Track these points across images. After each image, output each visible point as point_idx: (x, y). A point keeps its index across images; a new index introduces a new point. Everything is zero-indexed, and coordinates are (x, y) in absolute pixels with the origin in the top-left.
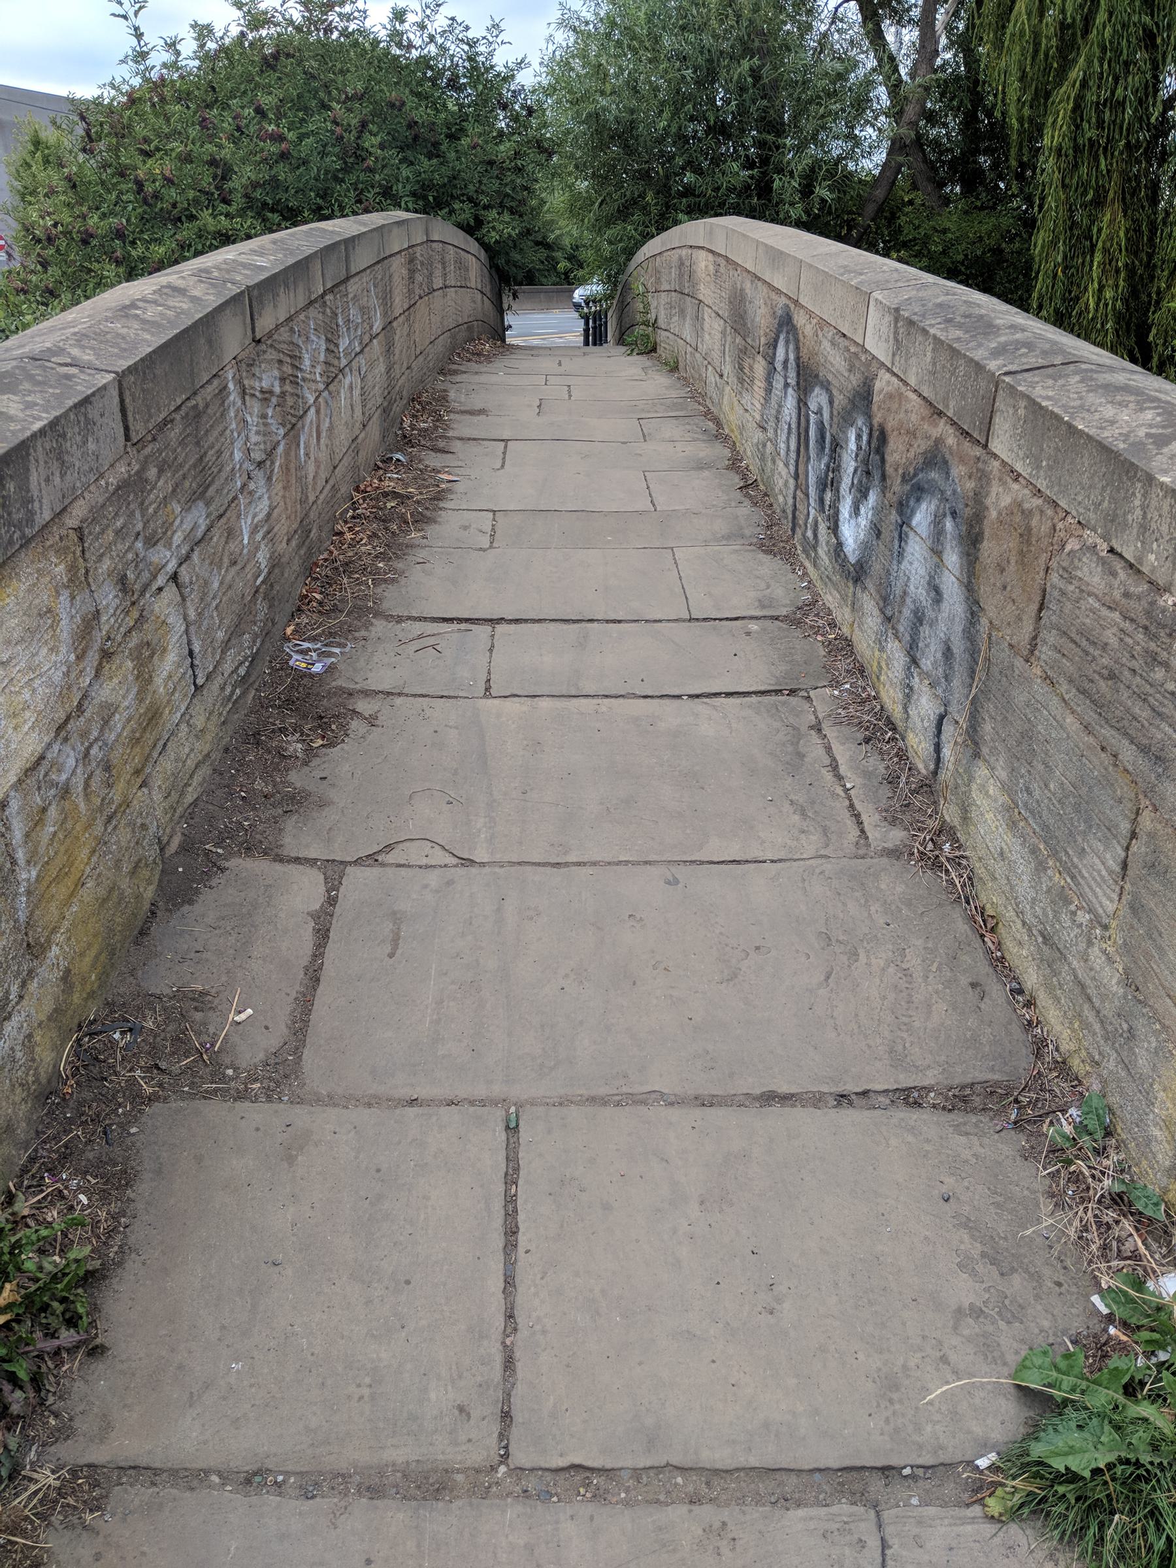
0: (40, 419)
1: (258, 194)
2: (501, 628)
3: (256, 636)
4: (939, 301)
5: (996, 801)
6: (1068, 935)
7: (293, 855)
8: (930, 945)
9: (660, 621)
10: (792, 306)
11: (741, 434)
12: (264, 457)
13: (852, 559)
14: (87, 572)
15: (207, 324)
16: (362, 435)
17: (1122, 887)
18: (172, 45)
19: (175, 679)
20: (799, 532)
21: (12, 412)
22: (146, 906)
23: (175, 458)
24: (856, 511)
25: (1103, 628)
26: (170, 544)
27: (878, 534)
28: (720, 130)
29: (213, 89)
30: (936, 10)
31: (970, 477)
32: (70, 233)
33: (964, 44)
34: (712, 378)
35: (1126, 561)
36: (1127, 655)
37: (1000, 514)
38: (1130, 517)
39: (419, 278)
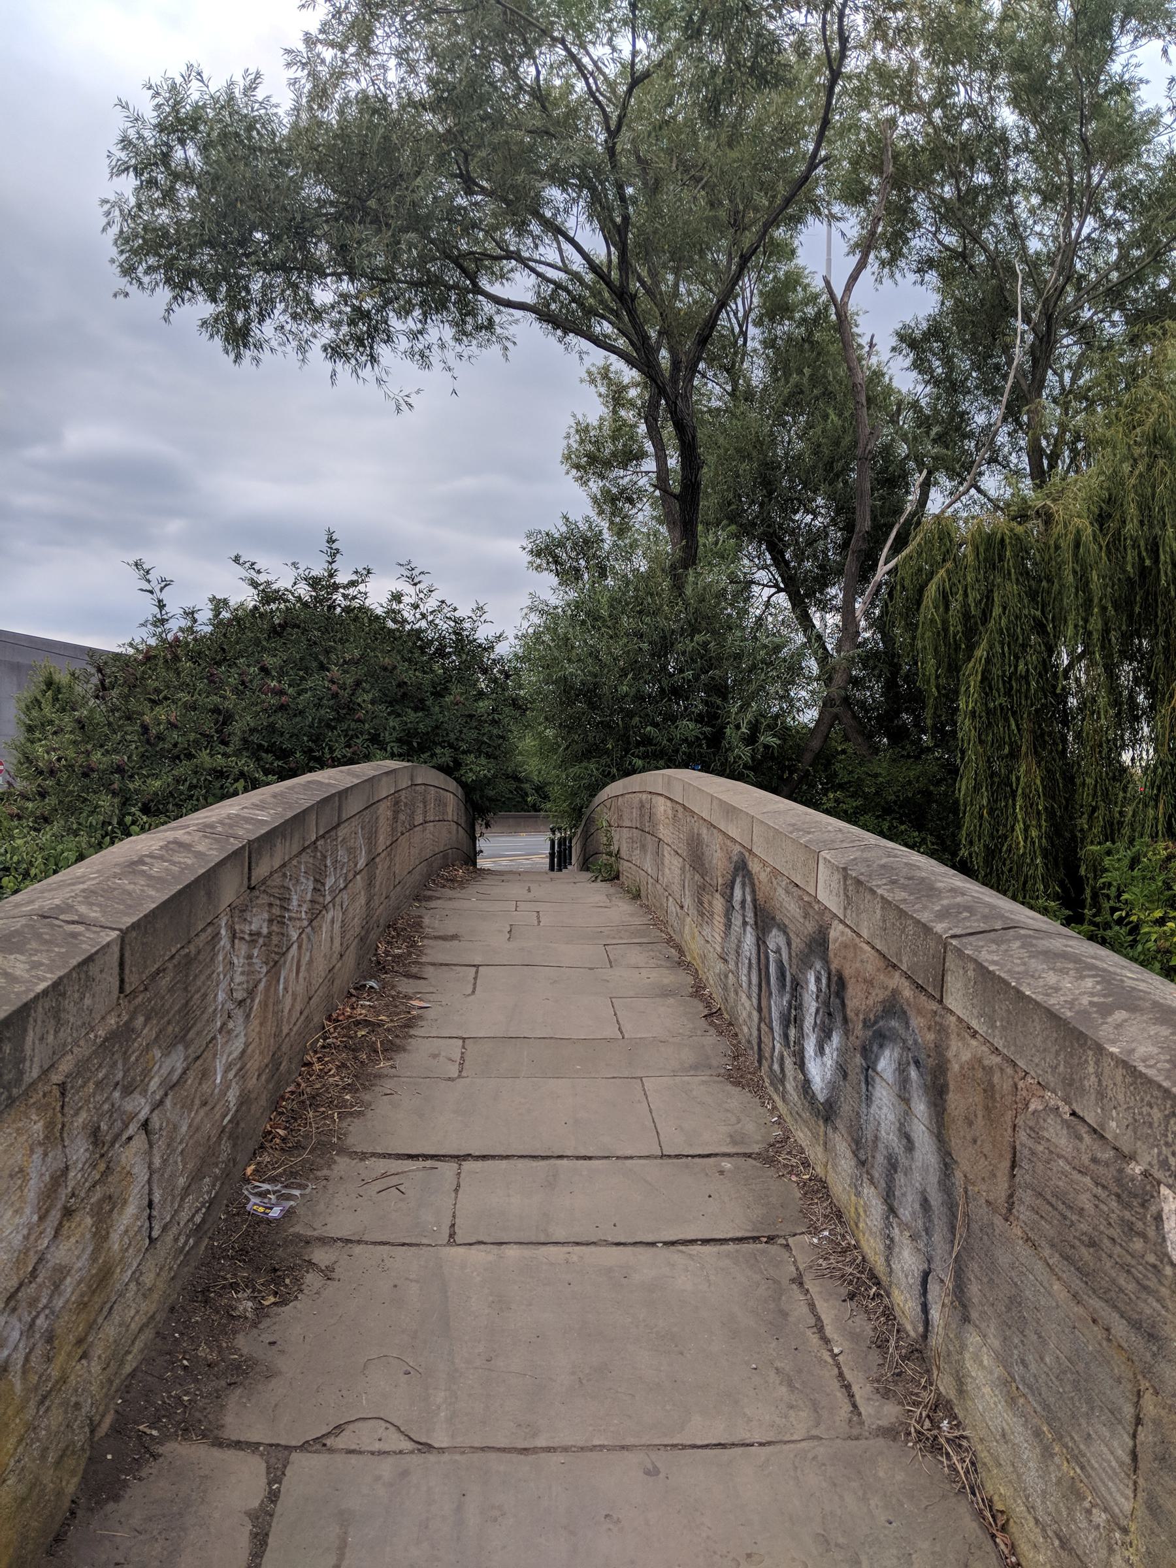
0: (44, 979)
1: (255, 738)
2: (468, 1165)
3: (216, 1178)
4: (883, 861)
6: (1086, 1540)
7: (234, 1438)
8: (938, 1549)
9: (631, 1158)
10: (747, 854)
11: (703, 962)
12: (245, 995)
13: (821, 1098)
14: (63, 1126)
15: (207, 882)
16: (339, 965)
17: (1135, 1483)
18: (190, 614)
19: (131, 1233)
20: (765, 1064)
21: (18, 973)
22: (67, 1504)
23: (163, 1005)
24: (821, 1051)
26: (146, 1091)
27: (845, 1076)
28: (677, 692)
29: (223, 650)
30: (855, 600)
31: (929, 1029)
32: (72, 766)
33: (881, 625)
34: (673, 908)
35: (1089, 1126)
36: (1105, 1223)
37: (962, 1067)
38: (1086, 1082)
39: (402, 817)
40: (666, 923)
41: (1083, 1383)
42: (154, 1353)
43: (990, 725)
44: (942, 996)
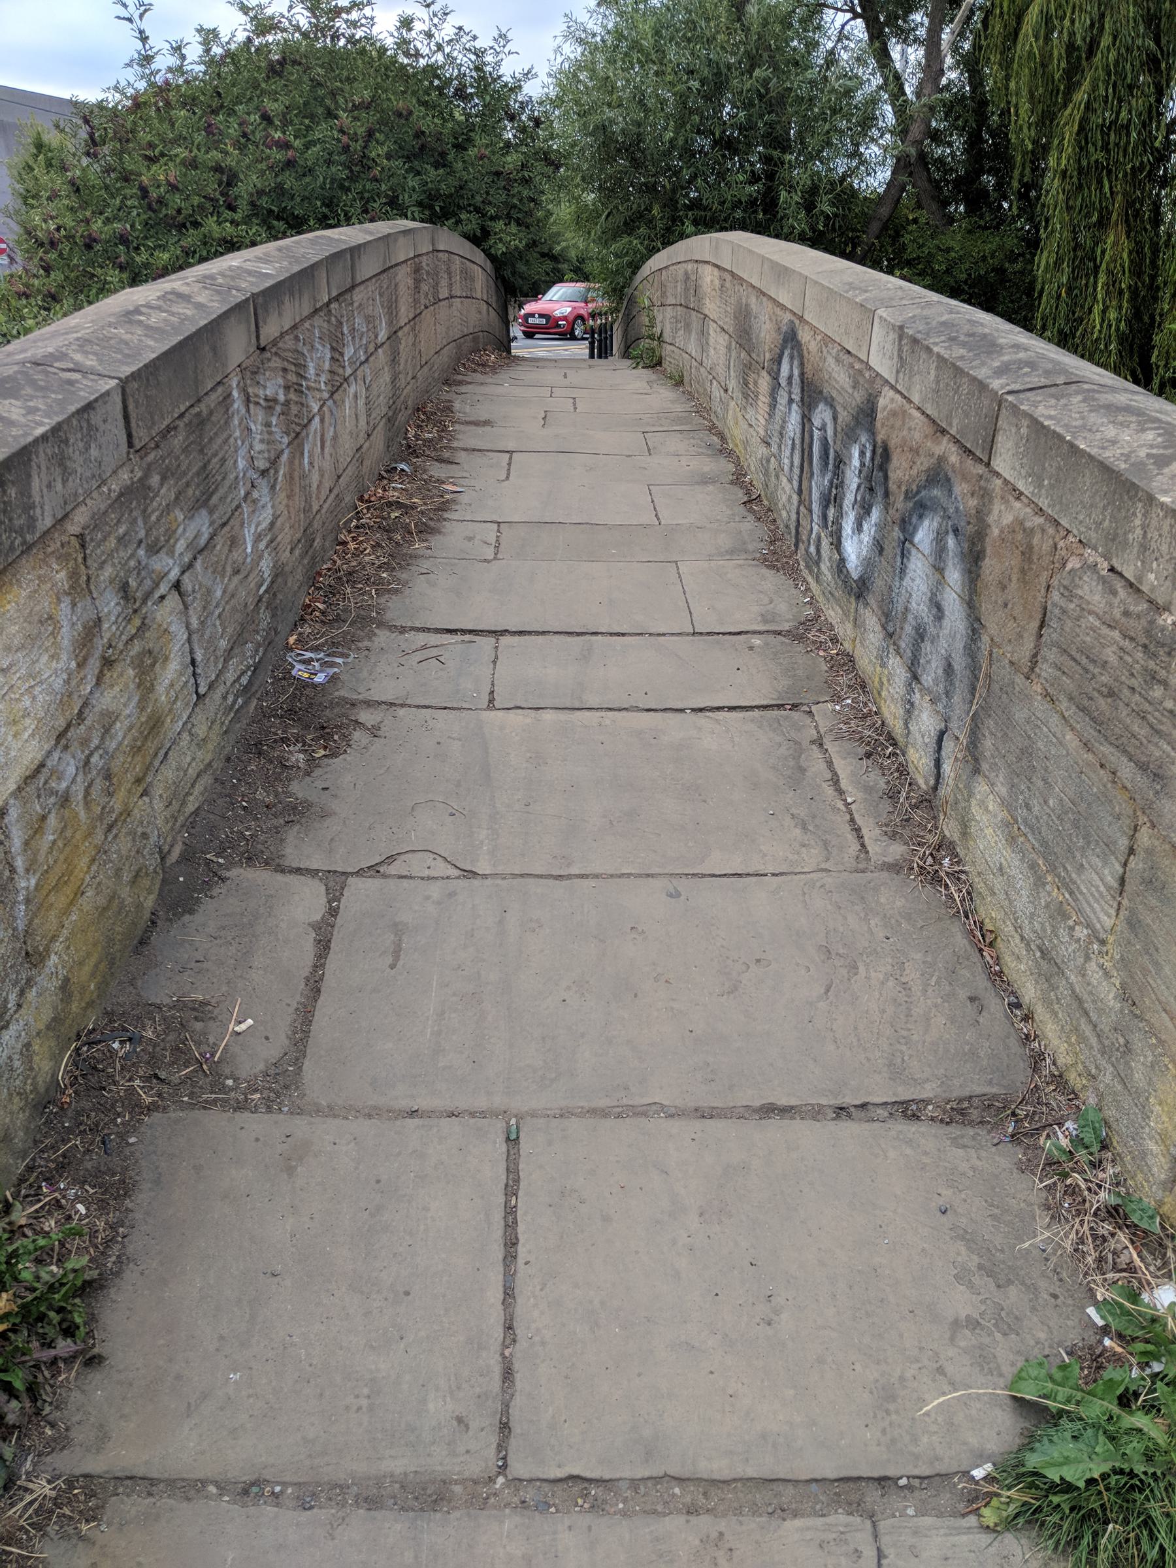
0: (41, 424)
1: (264, 202)
2: (505, 640)
3: (259, 645)
4: (943, 319)
5: (995, 816)
8: (929, 959)
9: (664, 635)
10: (797, 322)
11: (745, 449)
12: (268, 465)
13: (855, 575)
15: (211, 332)
17: (1120, 903)
19: (177, 687)
20: (802, 547)
21: (14, 417)
22: (147, 915)
23: (179, 465)
24: (859, 528)
25: (1103, 646)
27: (881, 551)
28: (727, 145)
29: (219, 94)
31: (972, 495)
32: (73, 237)
33: (971, 65)
34: (717, 392)
35: (1127, 580)
36: (1127, 674)
37: (1002, 532)
38: (1130, 536)
39: (425, 287)
40: (708, 410)
41: (1083, 821)
42: (215, 796)
43: (1080, 187)
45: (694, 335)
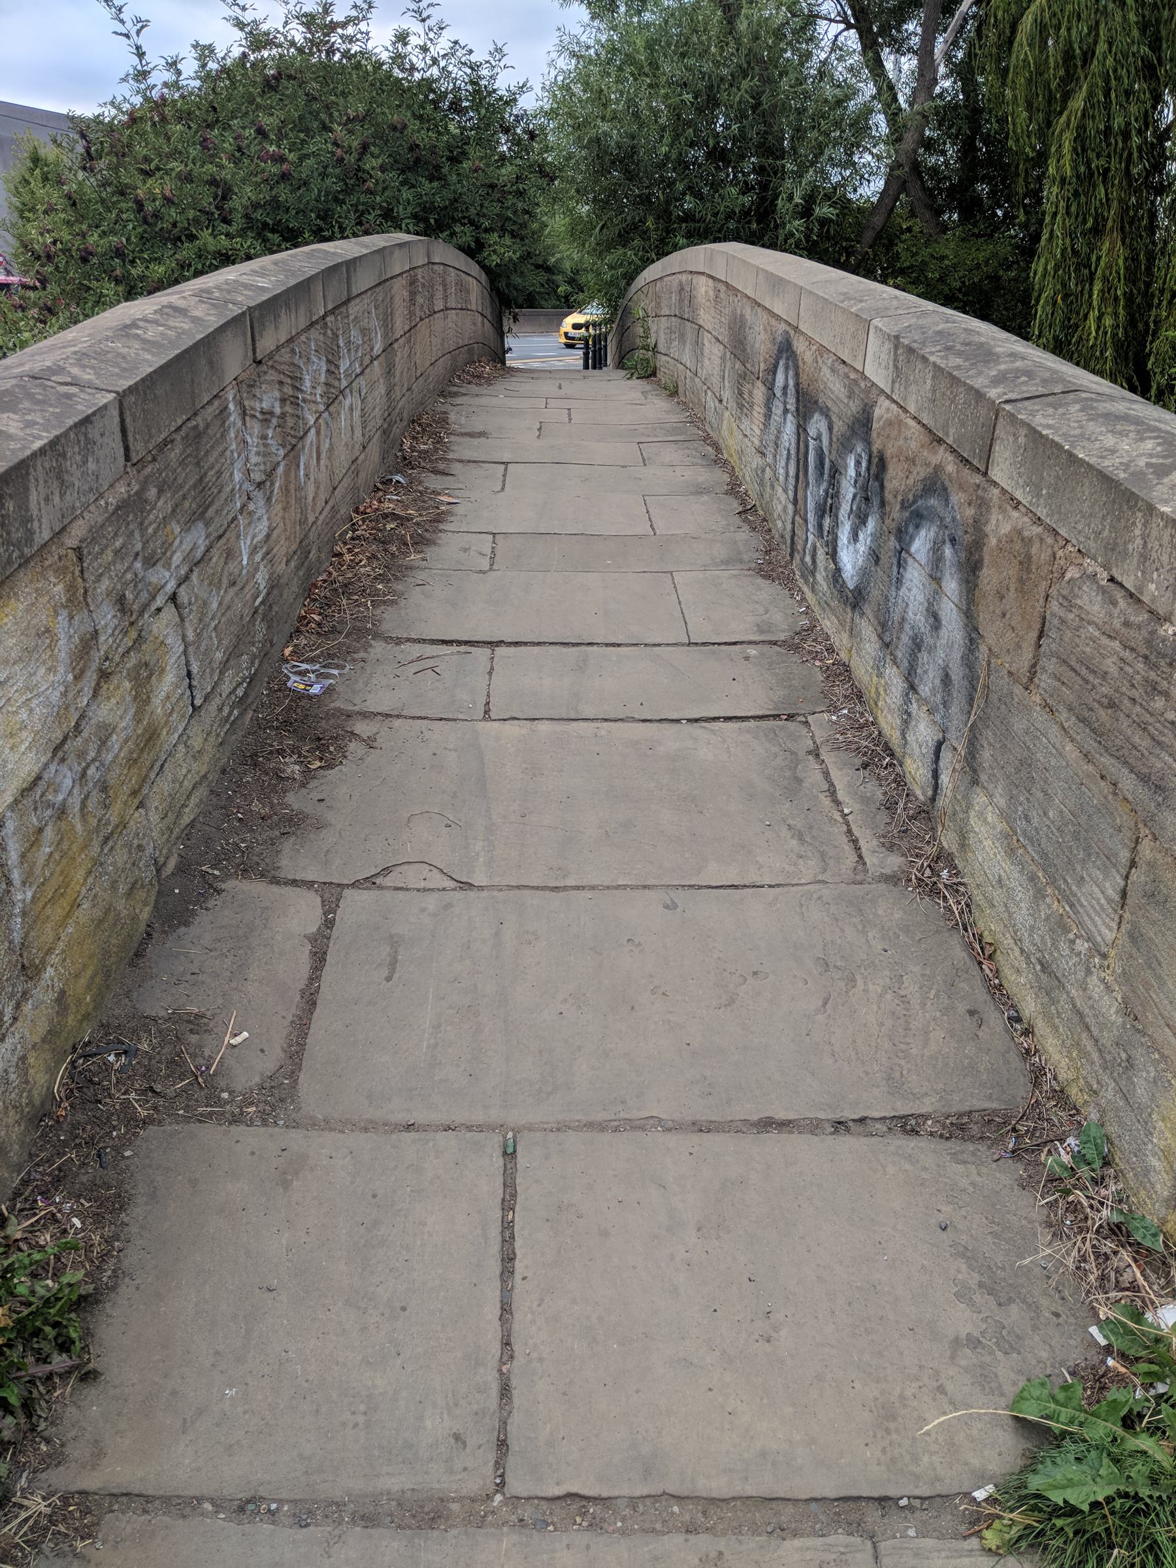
0: (40, 438)
1: (258, 215)
2: (501, 651)
3: (254, 657)
4: (940, 328)
5: (994, 828)
6: (1066, 964)
9: (659, 645)
11: (740, 459)
12: (264, 477)
13: (851, 585)
14: (86, 592)
16: (362, 457)
17: (1121, 917)
18: (173, 65)
19: (173, 700)
20: (797, 557)
21: (12, 431)
22: (143, 927)
23: (175, 479)
24: (855, 537)
25: (1103, 657)
26: (170, 565)
27: (877, 560)
29: (214, 109)
31: (970, 504)
33: (964, 72)
34: (711, 403)
35: (1127, 590)
36: (1128, 684)
37: (999, 541)
38: (1130, 547)
39: (420, 300)
44: (987, 468)
45: (688, 347)
